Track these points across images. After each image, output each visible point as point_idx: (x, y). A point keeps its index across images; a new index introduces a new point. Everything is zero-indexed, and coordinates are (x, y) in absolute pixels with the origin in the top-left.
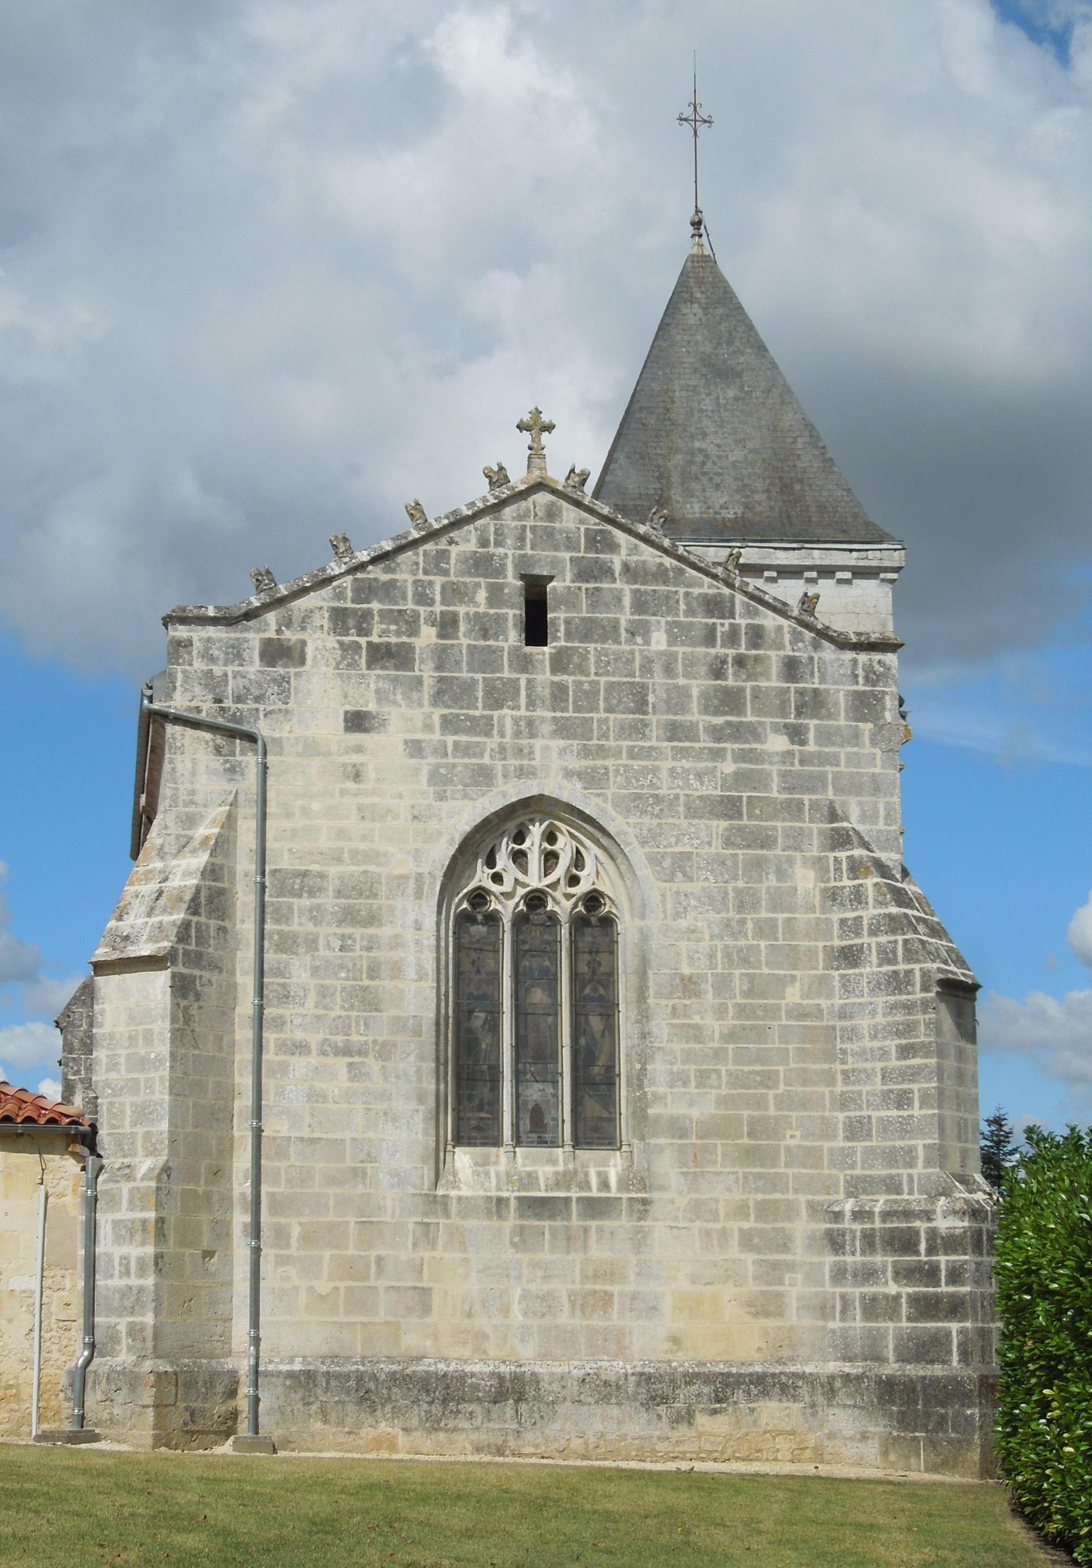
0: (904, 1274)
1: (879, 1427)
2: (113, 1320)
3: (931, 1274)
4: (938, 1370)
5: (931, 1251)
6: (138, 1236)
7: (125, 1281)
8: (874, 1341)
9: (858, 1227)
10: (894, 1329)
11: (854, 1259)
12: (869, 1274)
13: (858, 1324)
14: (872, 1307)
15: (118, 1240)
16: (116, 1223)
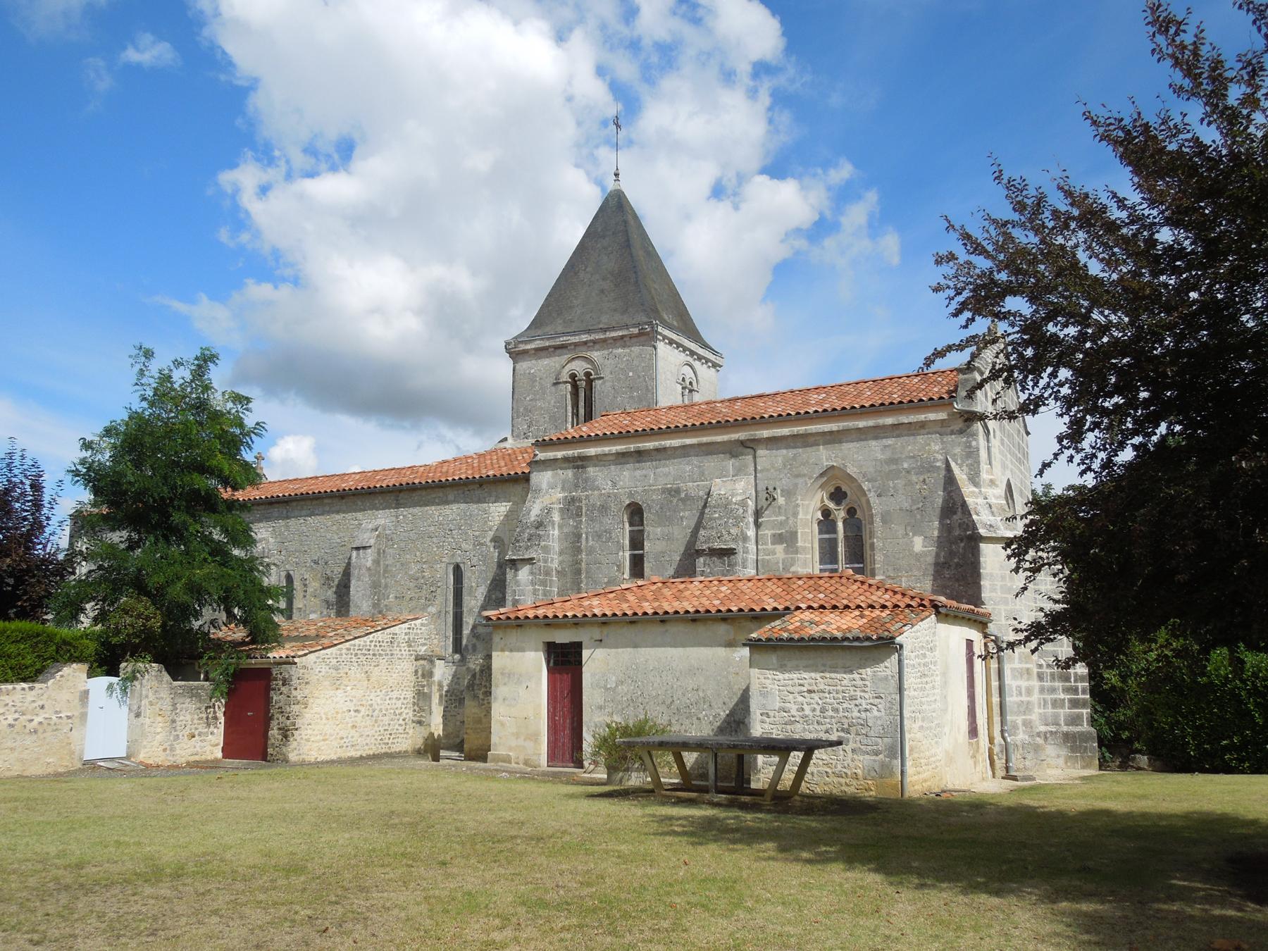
0: (1067, 690)
1: (1064, 752)
2: (1014, 718)
3: (1075, 690)
4: (1079, 729)
5: (1076, 681)
6: (1025, 676)
7: (1020, 698)
8: (1056, 716)
9: (1049, 671)
10: (1065, 712)
11: (1047, 684)
12: (1053, 690)
13: (1050, 710)
14: (1056, 704)
15: (1014, 678)
16: (1013, 670)
